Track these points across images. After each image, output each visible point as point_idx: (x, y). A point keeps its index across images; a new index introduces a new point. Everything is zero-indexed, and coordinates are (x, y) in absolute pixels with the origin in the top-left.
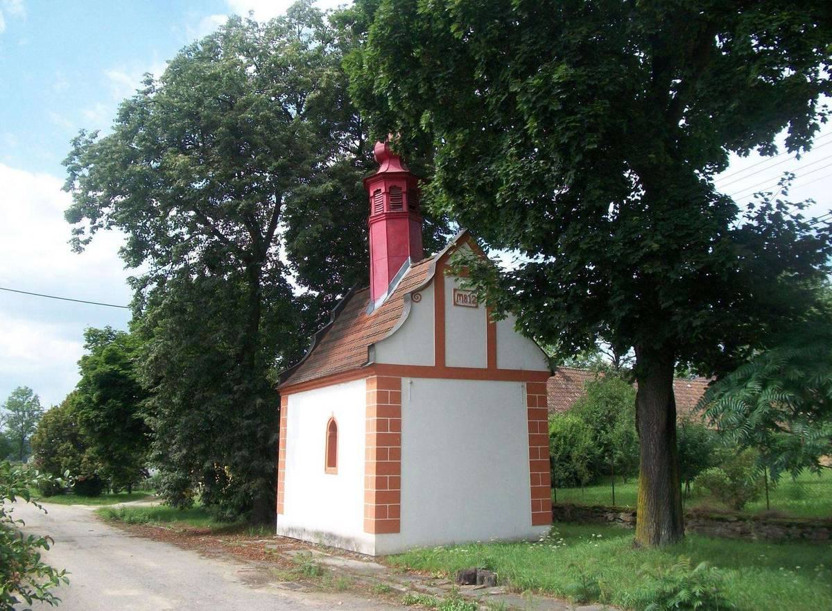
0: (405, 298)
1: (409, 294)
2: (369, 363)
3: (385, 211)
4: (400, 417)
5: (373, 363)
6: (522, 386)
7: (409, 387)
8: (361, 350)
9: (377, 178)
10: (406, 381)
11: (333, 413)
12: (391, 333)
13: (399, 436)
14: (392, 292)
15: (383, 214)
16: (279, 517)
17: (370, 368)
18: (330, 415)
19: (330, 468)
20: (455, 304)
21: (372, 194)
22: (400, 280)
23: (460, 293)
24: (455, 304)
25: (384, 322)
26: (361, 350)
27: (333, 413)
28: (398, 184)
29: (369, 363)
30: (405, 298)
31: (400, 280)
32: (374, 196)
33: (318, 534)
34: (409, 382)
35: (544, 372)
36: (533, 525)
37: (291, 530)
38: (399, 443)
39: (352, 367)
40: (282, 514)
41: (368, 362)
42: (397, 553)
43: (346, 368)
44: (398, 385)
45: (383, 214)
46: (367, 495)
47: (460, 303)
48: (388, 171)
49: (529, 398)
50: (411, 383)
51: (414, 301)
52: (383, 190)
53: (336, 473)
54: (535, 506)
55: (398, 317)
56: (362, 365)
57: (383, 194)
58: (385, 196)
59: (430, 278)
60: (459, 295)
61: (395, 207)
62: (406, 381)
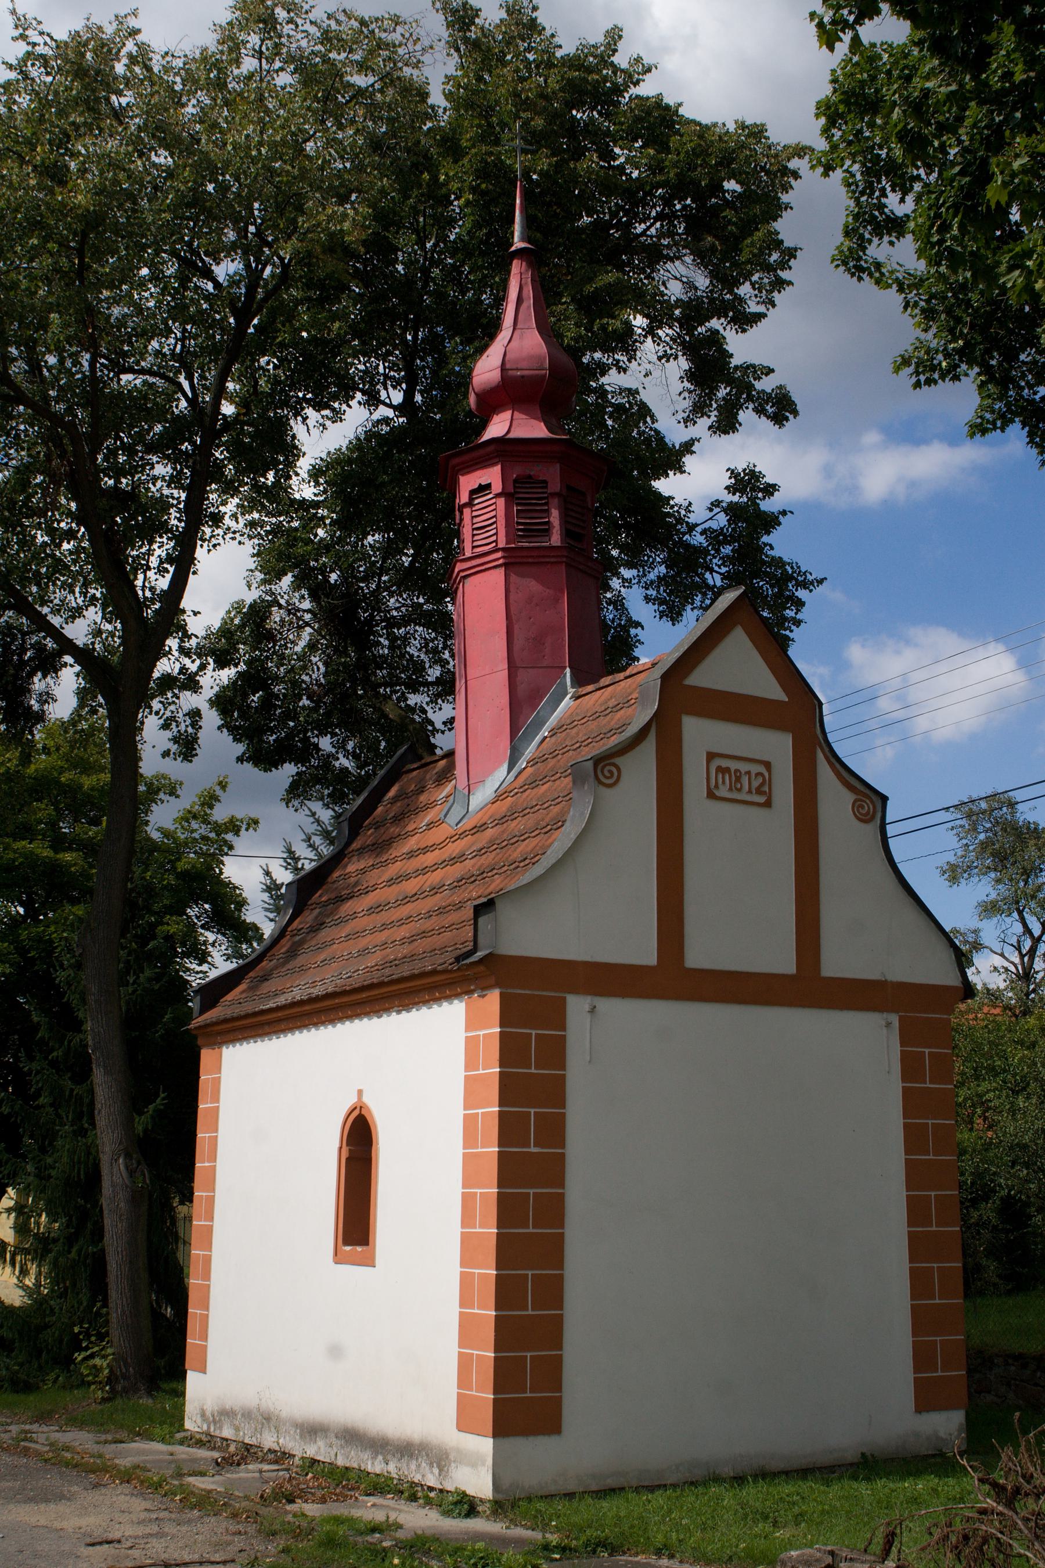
0: (577, 775)
1: (590, 764)
2: (480, 954)
3: (502, 544)
4: (564, 1107)
5: (490, 954)
6: (888, 1025)
7: (589, 1020)
8: (454, 917)
9: (482, 452)
10: (577, 1006)
11: (360, 1092)
12: (537, 870)
13: (560, 1160)
14: (522, 764)
15: (496, 550)
16: (193, 1380)
17: (482, 968)
18: (352, 1100)
19: (348, 1248)
20: (711, 795)
21: (464, 497)
22: (545, 732)
23: (724, 763)
24: (711, 795)
25: (522, 837)
26: (454, 917)
27: (360, 1092)
28: (537, 470)
29: (480, 954)
30: (577, 775)
31: (545, 732)
32: (470, 504)
33: (312, 1430)
34: (587, 1008)
35: (953, 987)
36: (205, 1372)
37: (226, 1414)
38: (559, 1180)
39: (417, 967)
40: (203, 1371)
41: (475, 950)
42: (571, 1487)
43: (405, 971)
44: (559, 1019)
45: (496, 550)
46: (466, 1327)
47: (723, 792)
48: (511, 435)
49: (905, 1057)
50: (593, 1010)
51: (600, 782)
52: (497, 487)
53: (369, 1261)
54: (922, 1358)
55: (559, 823)
56: (458, 959)
57: (497, 496)
58: (501, 502)
59: (647, 718)
60: (719, 769)
61: (530, 532)
62: (577, 1006)
